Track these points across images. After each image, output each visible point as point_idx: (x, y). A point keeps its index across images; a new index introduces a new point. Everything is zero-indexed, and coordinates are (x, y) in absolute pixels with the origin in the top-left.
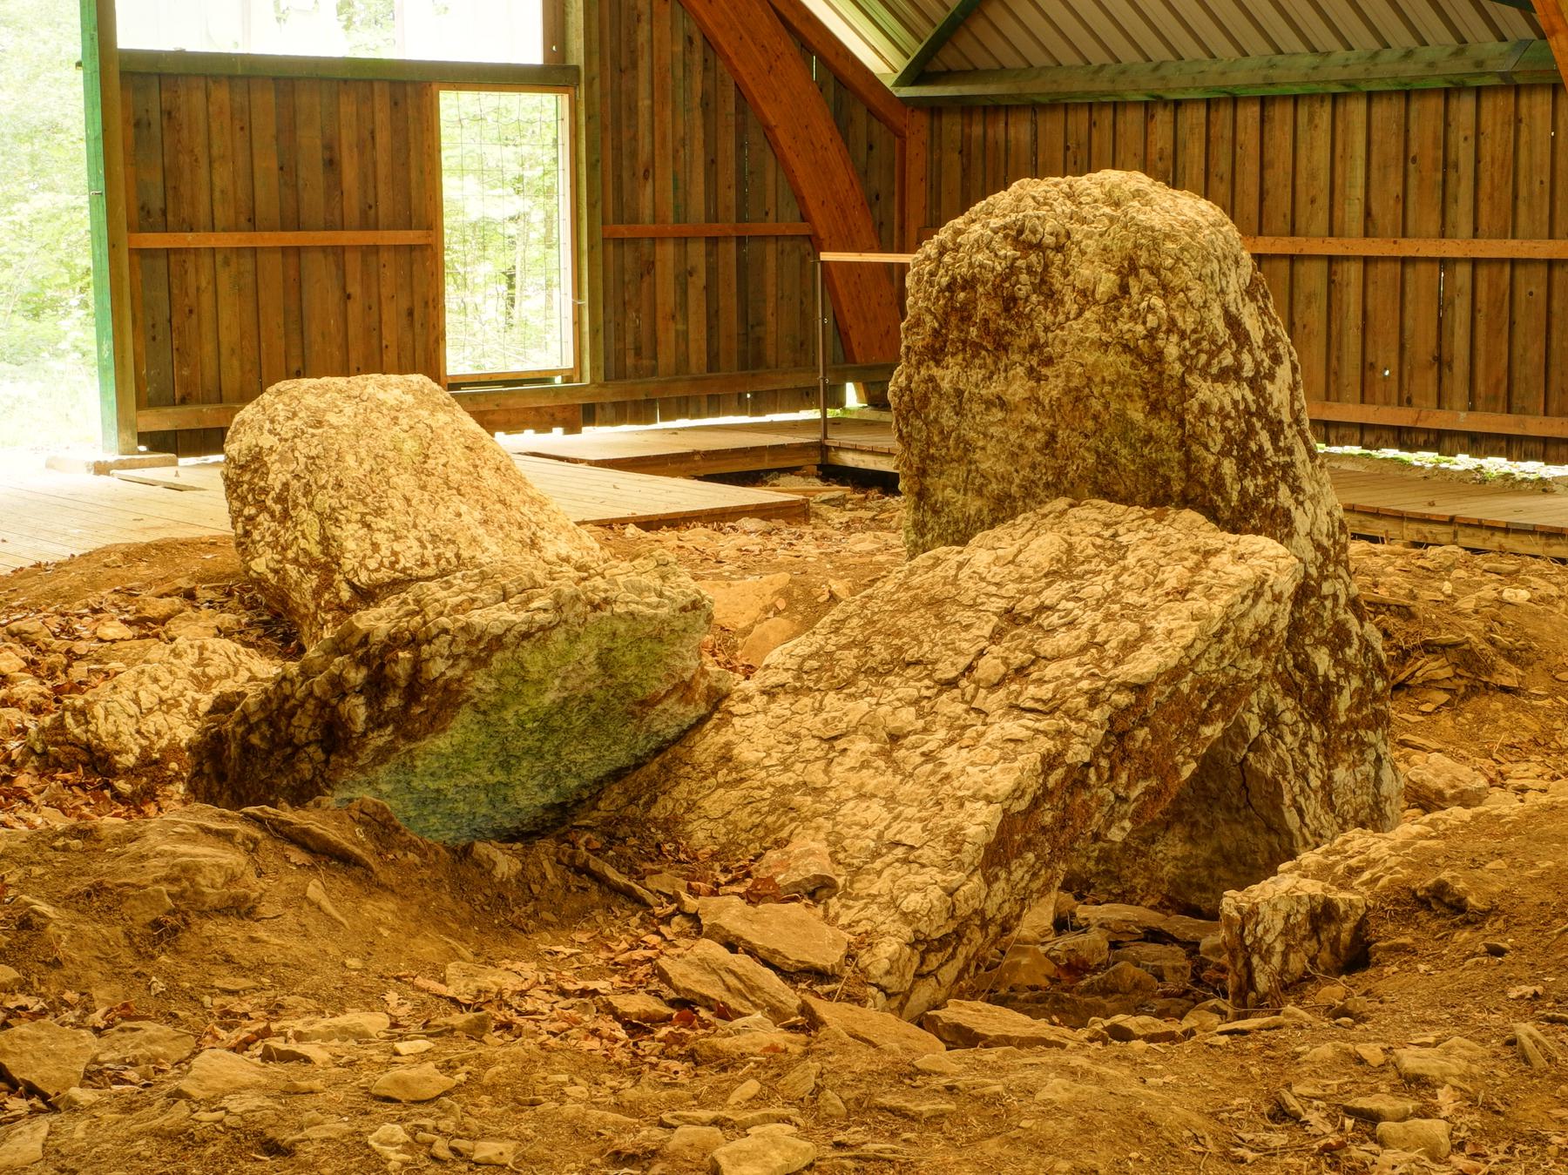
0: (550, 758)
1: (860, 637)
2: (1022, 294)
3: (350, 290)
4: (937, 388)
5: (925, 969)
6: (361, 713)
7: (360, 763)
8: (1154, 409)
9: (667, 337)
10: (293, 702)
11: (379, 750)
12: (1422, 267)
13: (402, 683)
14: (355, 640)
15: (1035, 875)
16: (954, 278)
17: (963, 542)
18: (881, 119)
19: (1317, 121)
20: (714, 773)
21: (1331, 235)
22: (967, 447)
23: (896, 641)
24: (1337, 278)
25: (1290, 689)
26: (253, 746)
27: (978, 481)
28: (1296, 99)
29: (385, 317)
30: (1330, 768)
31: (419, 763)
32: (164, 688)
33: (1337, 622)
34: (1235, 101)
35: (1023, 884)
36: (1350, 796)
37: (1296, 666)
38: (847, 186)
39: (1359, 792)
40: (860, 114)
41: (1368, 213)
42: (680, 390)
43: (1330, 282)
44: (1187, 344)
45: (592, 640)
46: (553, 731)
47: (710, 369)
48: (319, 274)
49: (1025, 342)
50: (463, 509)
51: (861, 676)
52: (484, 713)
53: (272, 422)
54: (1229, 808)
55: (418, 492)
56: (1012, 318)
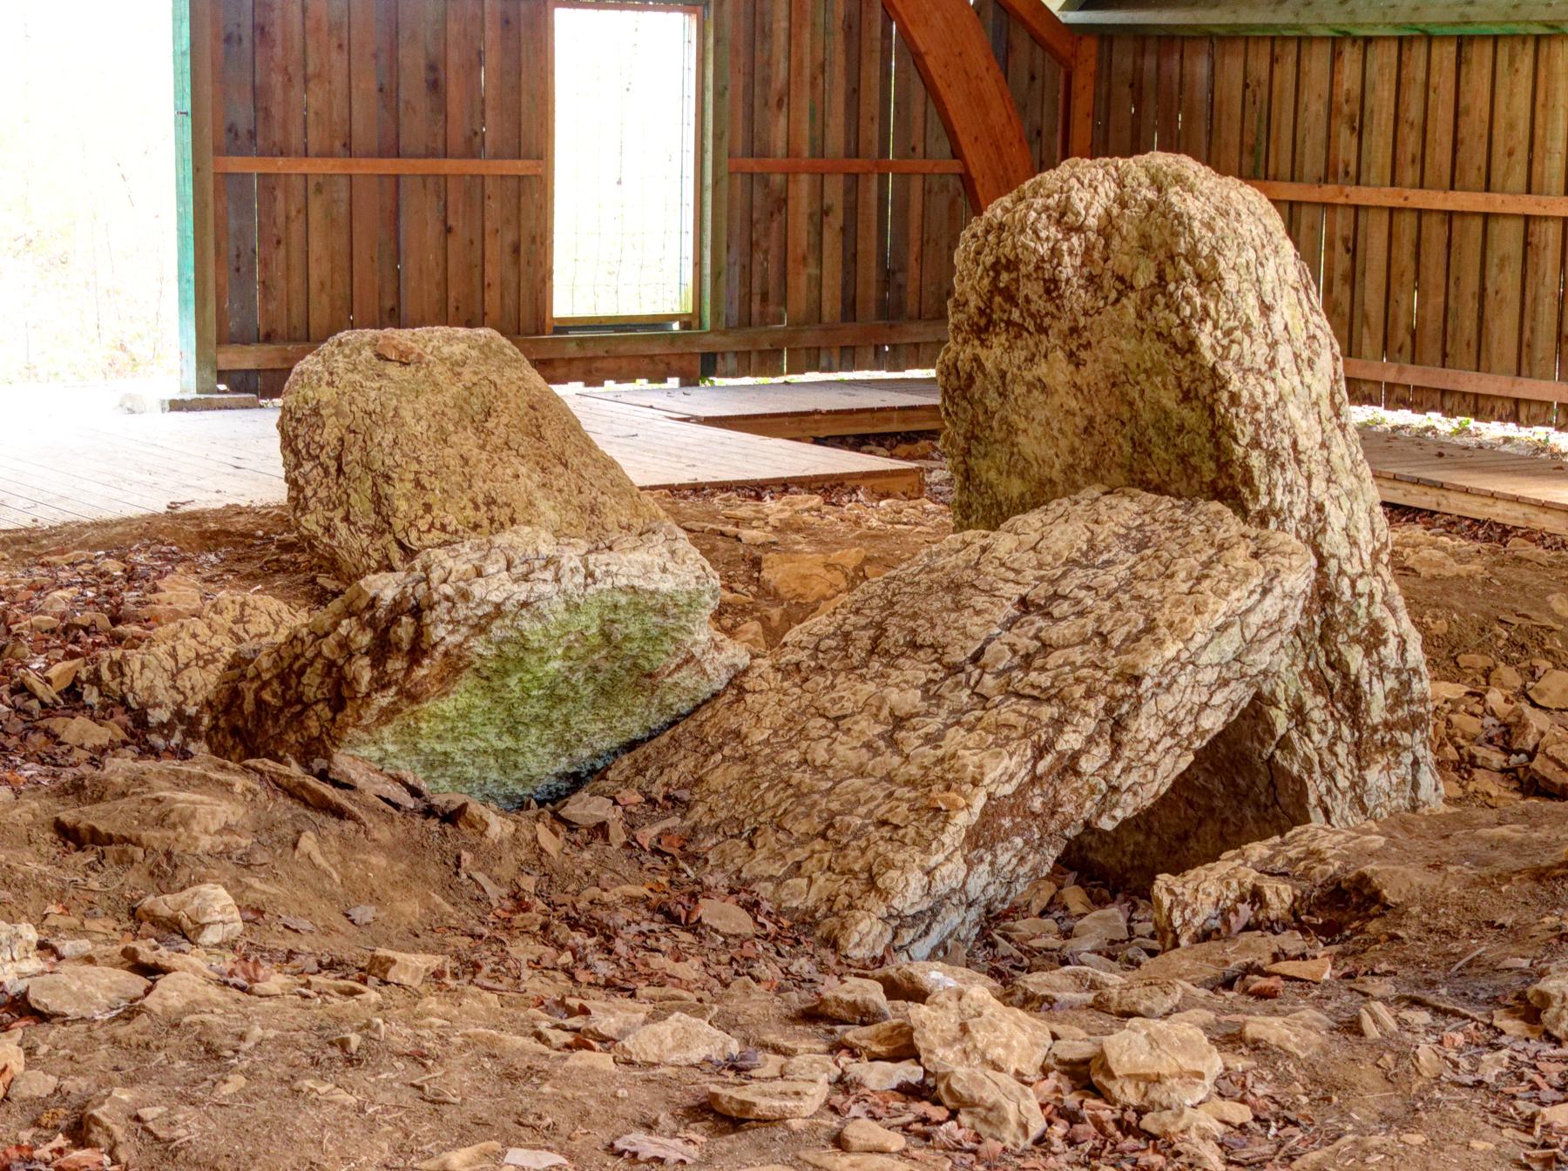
0: (559, 727)
1: (878, 618)
2: (1063, 277)
3: (451, 222)
4: (981, 366)
5: (897, 944)
6: (366, 676)
7: (364, 722)
8: (1186, 397)
9: (800, 283)
10: (302, 660)
11: (383, 711)
13: (405, 646)
14: (363, 603)
15: (1022, 860)
16: (998, 258)
17: (994, 526)
18: (1047, 47)
19: (1517, 65)
20: (720, 747)
21: (1529, 192)
22: (1012, 430)
23: (911, 624)
24: (1534, 240)
25: (1322, 687)
26: (264, 702)
27: (1021, 464)
28: (1496, 39)
29: (487, 254)
30: (1361, 769)
31: (423, 725)
32: (203, 644)
33: (1372, 621)
34: (1430, 39)
35: (1010, 867)
36: (1383, 799)
37: (1328, 663)
38: (1004, 121)
39: (1394, 795)
40: (1022, 43)
42: (810, 337)
43: (1527, 244)
44: (1219, 333)
45: (595, 612)
46: (562, 699)
47: (844, 318)
49: (1065, 325)
50: (523, 470)
51: (875, 657)
52: (487, 678)
53: (331, 374)
54: (1257, 805)
55: (476, 451)
56: (1052, 299)
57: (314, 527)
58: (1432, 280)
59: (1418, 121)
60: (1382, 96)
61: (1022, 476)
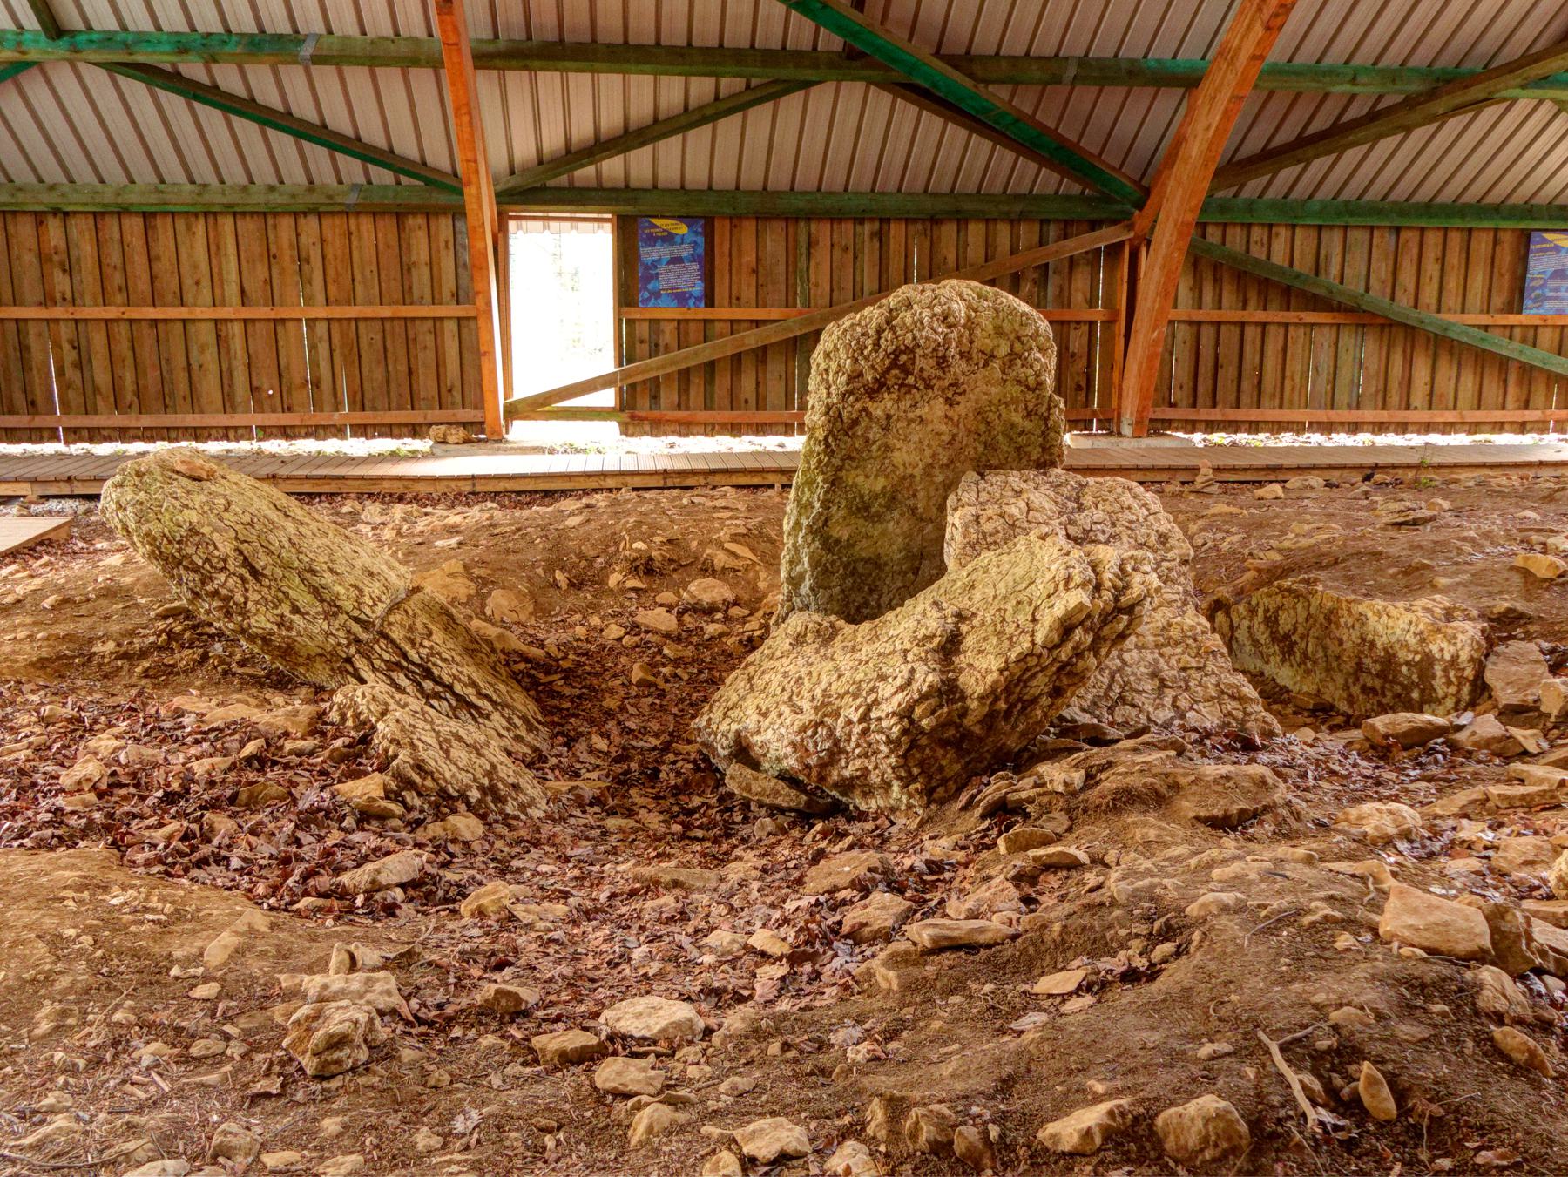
12: (203, 325)
24: (223, 334)
41: (243, 291)
48: (1251, 333)
57: (269, 625)
58: (148, 362)
59: (119, 264)
60: (87, 249)
61: (887, 477)
